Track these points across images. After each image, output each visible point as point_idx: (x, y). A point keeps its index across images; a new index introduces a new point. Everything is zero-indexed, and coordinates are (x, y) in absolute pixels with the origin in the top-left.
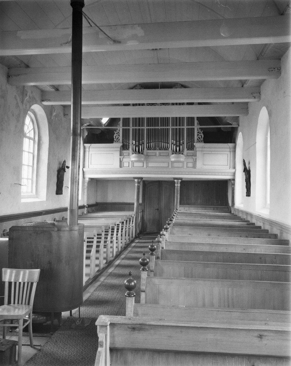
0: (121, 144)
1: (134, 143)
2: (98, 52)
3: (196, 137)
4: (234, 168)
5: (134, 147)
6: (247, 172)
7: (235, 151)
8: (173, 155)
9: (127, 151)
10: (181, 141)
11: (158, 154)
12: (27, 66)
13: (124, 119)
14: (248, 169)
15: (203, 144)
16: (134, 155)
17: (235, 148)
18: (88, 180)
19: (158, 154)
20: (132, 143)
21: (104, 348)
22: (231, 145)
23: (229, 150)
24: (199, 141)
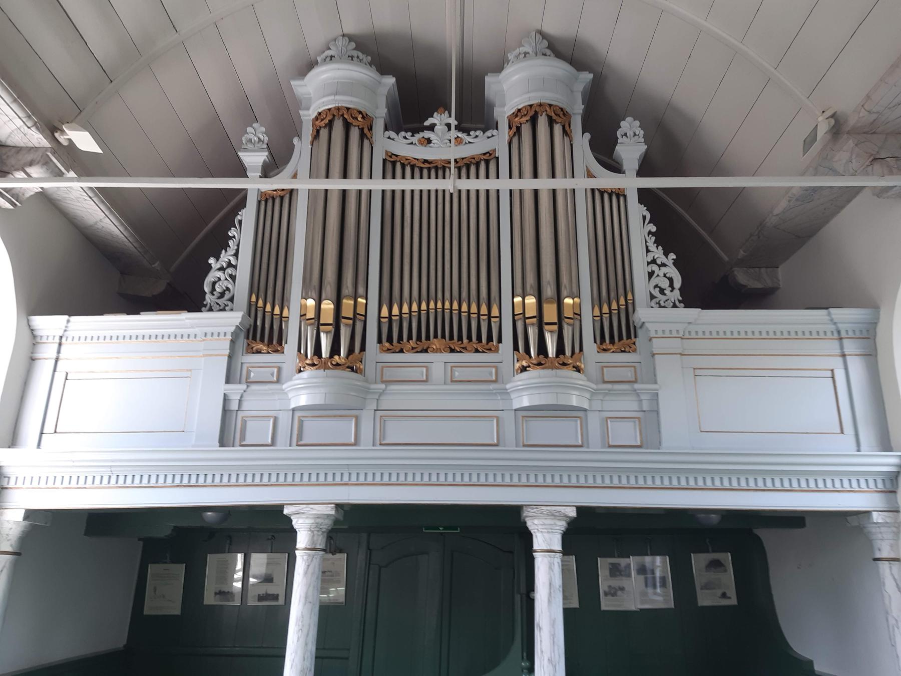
3: (641, 286)
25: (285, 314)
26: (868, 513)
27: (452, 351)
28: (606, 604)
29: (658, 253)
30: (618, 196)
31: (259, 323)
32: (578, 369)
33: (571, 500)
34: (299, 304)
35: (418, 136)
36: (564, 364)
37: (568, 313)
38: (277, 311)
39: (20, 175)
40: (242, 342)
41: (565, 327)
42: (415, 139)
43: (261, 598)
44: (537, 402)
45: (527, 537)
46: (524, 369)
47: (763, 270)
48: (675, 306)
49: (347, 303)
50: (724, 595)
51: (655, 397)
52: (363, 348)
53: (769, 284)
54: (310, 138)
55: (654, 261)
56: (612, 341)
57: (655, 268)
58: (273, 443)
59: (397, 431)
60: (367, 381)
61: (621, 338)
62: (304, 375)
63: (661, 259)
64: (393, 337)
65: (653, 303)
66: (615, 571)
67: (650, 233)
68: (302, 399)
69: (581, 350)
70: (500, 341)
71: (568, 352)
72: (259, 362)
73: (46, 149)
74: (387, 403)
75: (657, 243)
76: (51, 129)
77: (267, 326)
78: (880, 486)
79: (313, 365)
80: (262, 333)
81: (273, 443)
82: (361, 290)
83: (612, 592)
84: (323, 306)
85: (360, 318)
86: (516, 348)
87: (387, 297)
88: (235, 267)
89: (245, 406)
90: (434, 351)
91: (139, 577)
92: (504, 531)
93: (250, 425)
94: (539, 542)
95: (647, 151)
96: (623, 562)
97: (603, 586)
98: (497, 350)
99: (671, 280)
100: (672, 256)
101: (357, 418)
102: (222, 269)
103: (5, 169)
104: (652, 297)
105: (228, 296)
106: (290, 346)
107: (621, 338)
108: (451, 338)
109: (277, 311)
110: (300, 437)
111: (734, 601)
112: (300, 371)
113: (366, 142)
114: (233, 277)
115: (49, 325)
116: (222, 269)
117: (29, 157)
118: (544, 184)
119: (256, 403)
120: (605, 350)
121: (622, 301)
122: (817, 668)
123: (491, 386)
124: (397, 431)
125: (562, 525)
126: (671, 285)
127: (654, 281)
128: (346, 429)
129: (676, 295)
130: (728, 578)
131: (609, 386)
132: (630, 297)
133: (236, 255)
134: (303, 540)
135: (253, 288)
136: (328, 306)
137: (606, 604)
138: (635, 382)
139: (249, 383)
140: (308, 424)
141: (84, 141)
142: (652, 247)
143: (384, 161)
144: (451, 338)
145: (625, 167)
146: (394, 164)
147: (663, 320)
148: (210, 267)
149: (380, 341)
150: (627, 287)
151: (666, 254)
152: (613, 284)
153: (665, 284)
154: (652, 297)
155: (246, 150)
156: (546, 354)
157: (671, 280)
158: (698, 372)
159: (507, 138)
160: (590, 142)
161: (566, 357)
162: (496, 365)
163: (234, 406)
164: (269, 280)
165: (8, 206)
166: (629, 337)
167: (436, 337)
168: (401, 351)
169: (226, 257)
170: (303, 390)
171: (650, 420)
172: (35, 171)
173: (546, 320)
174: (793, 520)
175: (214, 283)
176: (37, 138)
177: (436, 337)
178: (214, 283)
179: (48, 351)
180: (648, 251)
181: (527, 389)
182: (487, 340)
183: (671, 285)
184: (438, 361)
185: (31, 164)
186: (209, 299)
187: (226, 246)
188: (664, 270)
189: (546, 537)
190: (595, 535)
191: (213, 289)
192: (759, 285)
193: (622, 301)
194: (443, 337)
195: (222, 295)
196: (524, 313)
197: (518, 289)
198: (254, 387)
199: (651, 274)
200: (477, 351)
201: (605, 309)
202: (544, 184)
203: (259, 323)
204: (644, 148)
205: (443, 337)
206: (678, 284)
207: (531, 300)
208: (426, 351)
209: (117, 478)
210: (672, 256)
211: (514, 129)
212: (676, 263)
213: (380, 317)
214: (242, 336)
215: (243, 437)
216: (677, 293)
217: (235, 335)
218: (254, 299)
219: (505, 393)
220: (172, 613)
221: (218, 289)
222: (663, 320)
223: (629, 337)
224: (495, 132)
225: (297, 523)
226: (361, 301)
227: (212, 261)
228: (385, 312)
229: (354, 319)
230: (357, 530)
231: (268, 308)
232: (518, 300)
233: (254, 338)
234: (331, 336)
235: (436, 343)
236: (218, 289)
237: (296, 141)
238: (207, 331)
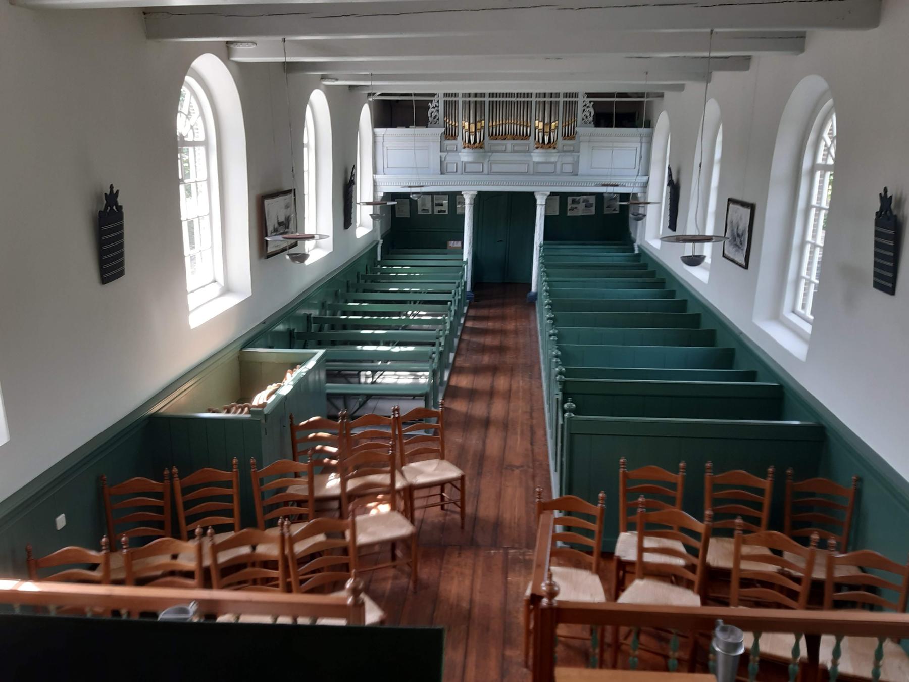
0: (443, 130)
1: (467, 127)
2: (547, 448)
3: (580, 115)
4: (647, 174)
5: (467, 134)
6: (675, 189)
7: (650, 143)
8: (537, 150)
9: (454, 142)
10: (553, 124)
11: (509, 147)
12: (316, 511)
13: (485, 202)
14: (675, 181)
15: (593, 130)
16: (466, 150)
17: (650, 137)
18: (382, 195)
19: (509, 147)
20: (463, 127)
21: (364, 192)
22: (643, 131)
23: (639, 139)
24: (585, 124)
28: (569, 214)
33: (548, 190)
37: (553, 127)
40: (444, 137)
43: (439, 212)
45: (535, 200)
51: (579, 156)
74: (492, 158)
83: (572, 209)
91: (896, 259)
92: (529, 199)
94: (538, 202)
97: (569, 207)
115: (380, 131)
119: (450, 158)
124: (496, 168)
125: (545, 197)
129: (591, 119)
134: (467, 201)
135: (445, 115)
139: (448, 151)
147: (586, 131)
161: (551, 145)
162: (528, 145)
170: (466, 156)
171: (576, 164)
181: (537, 156)
209: (413, 179)
219: (531, 156)
230: (482, 199)
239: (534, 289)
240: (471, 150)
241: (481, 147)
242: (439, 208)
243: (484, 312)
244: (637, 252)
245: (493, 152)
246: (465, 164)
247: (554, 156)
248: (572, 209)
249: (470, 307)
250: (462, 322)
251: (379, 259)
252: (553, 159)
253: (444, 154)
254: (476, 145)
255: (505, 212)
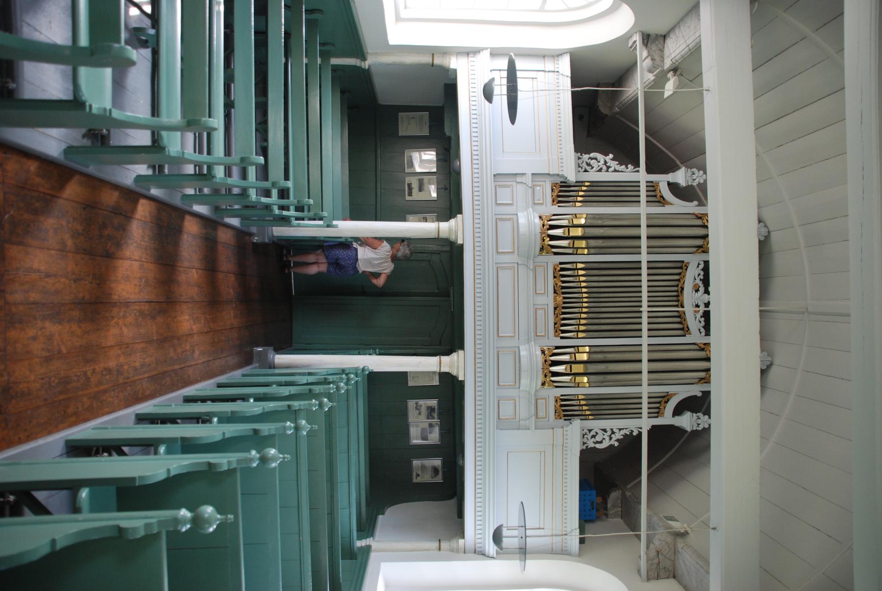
0: (572, 178)
1: (576, 222)
3: (597, 425)
9: (549, 199)
10: (585, 379)
17: (562, 553)
25: (578, 204)
26: (463, 537)
27: (555, 309)
28: (411, 404)
29: (618, 435)
30: (658, 413)
31: (572, 189)
32: (543, 384)
34: (581, 213)
35: (701, 284)
36: (546, 376)
37: (578, 379)
38: (579, 199)
39: (645, 54)
41: (570, 377)
42: (698, 281)
43: (409, 185)
44: (524, 361)
46: (543, 352)
47: (620, 509)
48: (584, 443)
49: (583, 243)
50: (418, 475)
52: (556, 254)
53: (611, 512)
54: (696, 212)
55: (613, 433)
56: (562, 406)
57: (609, 433)
58: (497, 204)
59: (506, 277)
60: (535, 257)
61: (564, 411)
62: (537, 220)
63: (614, 437)
64: (560, 271)
65: (586, 431)
66: (431, 410)
67: (632, 431)
68: (522, 220)
69: (557, 387)
70: (562, 338)
71: (553, 379)
72: (545, 191)
73: (663, 67)
75: (625, 436)
76: (675, 70)
77: (571, 194)
78: (478, 545)
79: (543, 225)
80: (564, 191)
81: (497, 204)
82: (592, 251)
83: (418, 407)
84: (580, 229)
85: (575, 251)
86: (557, 348)
87: (590, 267)
88: (607, 171)
89: (519, 186)
90: (555, 297)
92: (450, 340)
93: (508, 190)
94: (445, 359)
95: (686, 431)
96: (435, 415)
97: (422, 402)
98: (556, 336)
99: (601, 442)
100: (616, 444)
101: (513, 252)
102: (606, 163)
103: (649, 45)
104: (590, 431)
105: (588, 168)
106: (556, 209)
107: (564, 411)
108: (564, 308)
109: (579, 199)
110: (501, 220)
111: (415, 480)
112: (540, 217)
113: (695, 249)
114: (600, 170)
115: (565, 65)
116: (606, 163)
117: (657, 58)
118: (645, 366)
120: (556, 401)
121: (588, 413)
122: (380, 517)
123: (533, 334)
124: (506, 277)
126: (597, 442)
127: (600, 433)
128: (506, 245)
129: (591, 444)
130: (427, 478)
131: (533, 402)
132: (591, 417)
133: (615, 171)
134: (444, 226)
135: (593, 184)
136: (579, 232)
137: (411, 404)
138: (537, 417)
139: (533, 188)
140: (509, 224)
141: (669, 88)
142: (622, 432)
143: (683, 262)
144: (564, 308)
145: (676, 417)
146: (681, 268)
147: (573, 437)
148: (606, 155)
149: (561, 263)
150: (597, 416)
151: (617, 440)
152: (600, 407)
153: (598, 438)
154: (590, 431)
155: (686, 172)
156: (551, 365)
157: (601, 442)
158: (543, 454)
159: (698, 342)
160: (696, 396)
161: (550, 376)
162: (546, 336)
163: (519, 179)
164: (598, 192)
165: (630, 45)
166: (565, 416)
167: (564, 298)
168: (555, 277)
169: (614, 164)
170: (529, 220)
172: (648, 62)
173: (573, 366)
174: (460, 514)
175: (596, 159)
176: (668, 64)
177: (564, 298)
178: (596, 159)
179: (549, 65)
180: (620, 430)
181: (531, 355)
182: (560, 330)
183: (597, 442)
184: (548, 300)
185: (652, 59)
186: (586, 157)
187: (621, 164)
188: (607, 438)
189: (448, 363)
190: (450, 390)
191: (592, 159)
192: (609, 505)
193: (588, 413)
194: (564, 303)
195: (588, 164)
196: (579, 352)
197: (593, 349)
198: (530, 191)
199: (605, 430)
200: (555, 324)
201: (583, 402)
202: (645, 366)
203: (572, 189)
204: (689, 429)
205: (564, 303)
206: (598, 446)
207: (585, 357)
208: (555, 292)
210: (616, 444)
211: (703, 346)
212: (611, 446)
213: (576, 263)
214: (563, 180)
215: (500, 186)
216: (592, 445)
217: (562, 176)
218: (587, 184)
219: (528, 341)
220: (400, 126)
221: (592, 162)
222: (573, 437)
223: (565, 416)
224: (703, 334)
225: (452, 221)
226: (586, 251)
227: (611, 156)
228: (580, 266)
229: (573, 247)
230: (451, 254)
231: (581, 193)
232: (587, 349)
233: (561, 186)
234: (562, 235)
235: (560, 299)
236: (592, 162)
237: (696, 203)
238: (564, 160)
239: (281, 359)
240: (538, 230)
241: (542, 249)
242: (415, 186)
243: (227, 263)
244: (359, 544)
245: (535, 270)
246: (513, 219)
247: (531, 380)
248: (418, 407)
249: (241, 234)
250: (199, 208)
251: (334, 61)
252: (525, 382)
253: (528, 180)
254: (549, 240)
255: (427, 297)
